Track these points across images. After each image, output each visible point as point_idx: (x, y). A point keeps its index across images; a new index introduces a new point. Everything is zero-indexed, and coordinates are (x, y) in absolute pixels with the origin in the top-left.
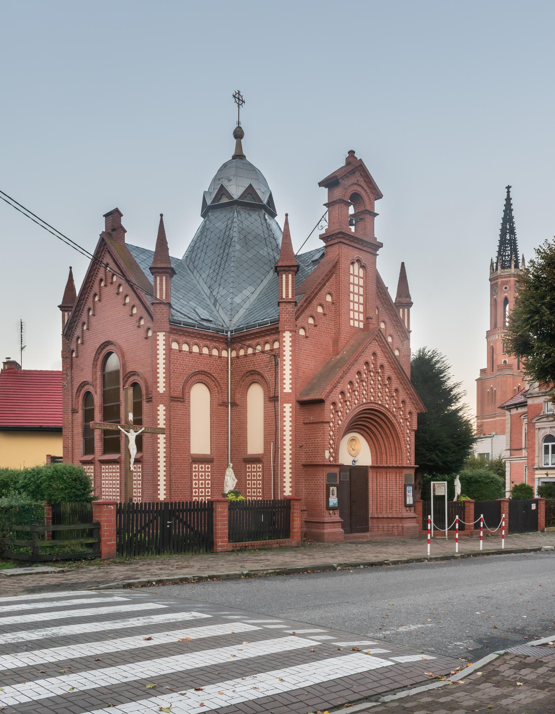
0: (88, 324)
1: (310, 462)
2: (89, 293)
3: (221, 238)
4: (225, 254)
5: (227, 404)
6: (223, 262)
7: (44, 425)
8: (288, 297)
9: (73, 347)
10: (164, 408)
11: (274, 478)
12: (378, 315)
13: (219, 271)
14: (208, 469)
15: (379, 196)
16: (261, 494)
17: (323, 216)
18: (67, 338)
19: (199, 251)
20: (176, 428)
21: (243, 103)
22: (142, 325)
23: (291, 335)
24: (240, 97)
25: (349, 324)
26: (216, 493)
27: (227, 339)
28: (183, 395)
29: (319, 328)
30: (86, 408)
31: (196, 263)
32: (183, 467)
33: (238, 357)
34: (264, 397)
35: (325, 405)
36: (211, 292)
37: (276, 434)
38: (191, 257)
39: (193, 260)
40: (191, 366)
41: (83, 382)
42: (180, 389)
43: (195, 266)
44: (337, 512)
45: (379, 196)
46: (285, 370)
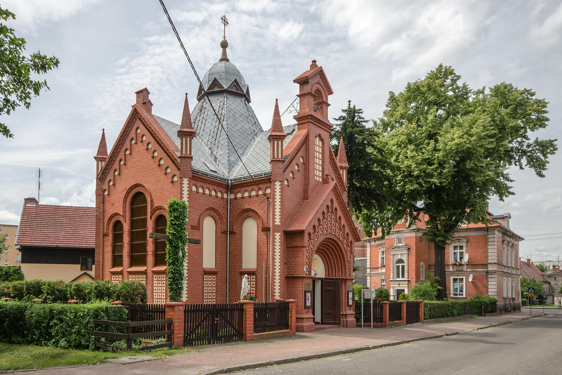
1: (292, 275)
5: (226, 232)
7: (60, 245)
8: (278, 157)
9: (105, 187)
13: (216, 138)
15: (331, 93)
18: (100, 180)
19: (200, 123)
22: (168, 173)
26: (219, 296)
27: (228, 185)
28: (199, 225)
30: (115, 233)
32: (198, 277)
36: (212, 152)
40: (204, 204)
41: (114, 213)
42: (197, 220)
45: (331, 93)
46: (276, 208)
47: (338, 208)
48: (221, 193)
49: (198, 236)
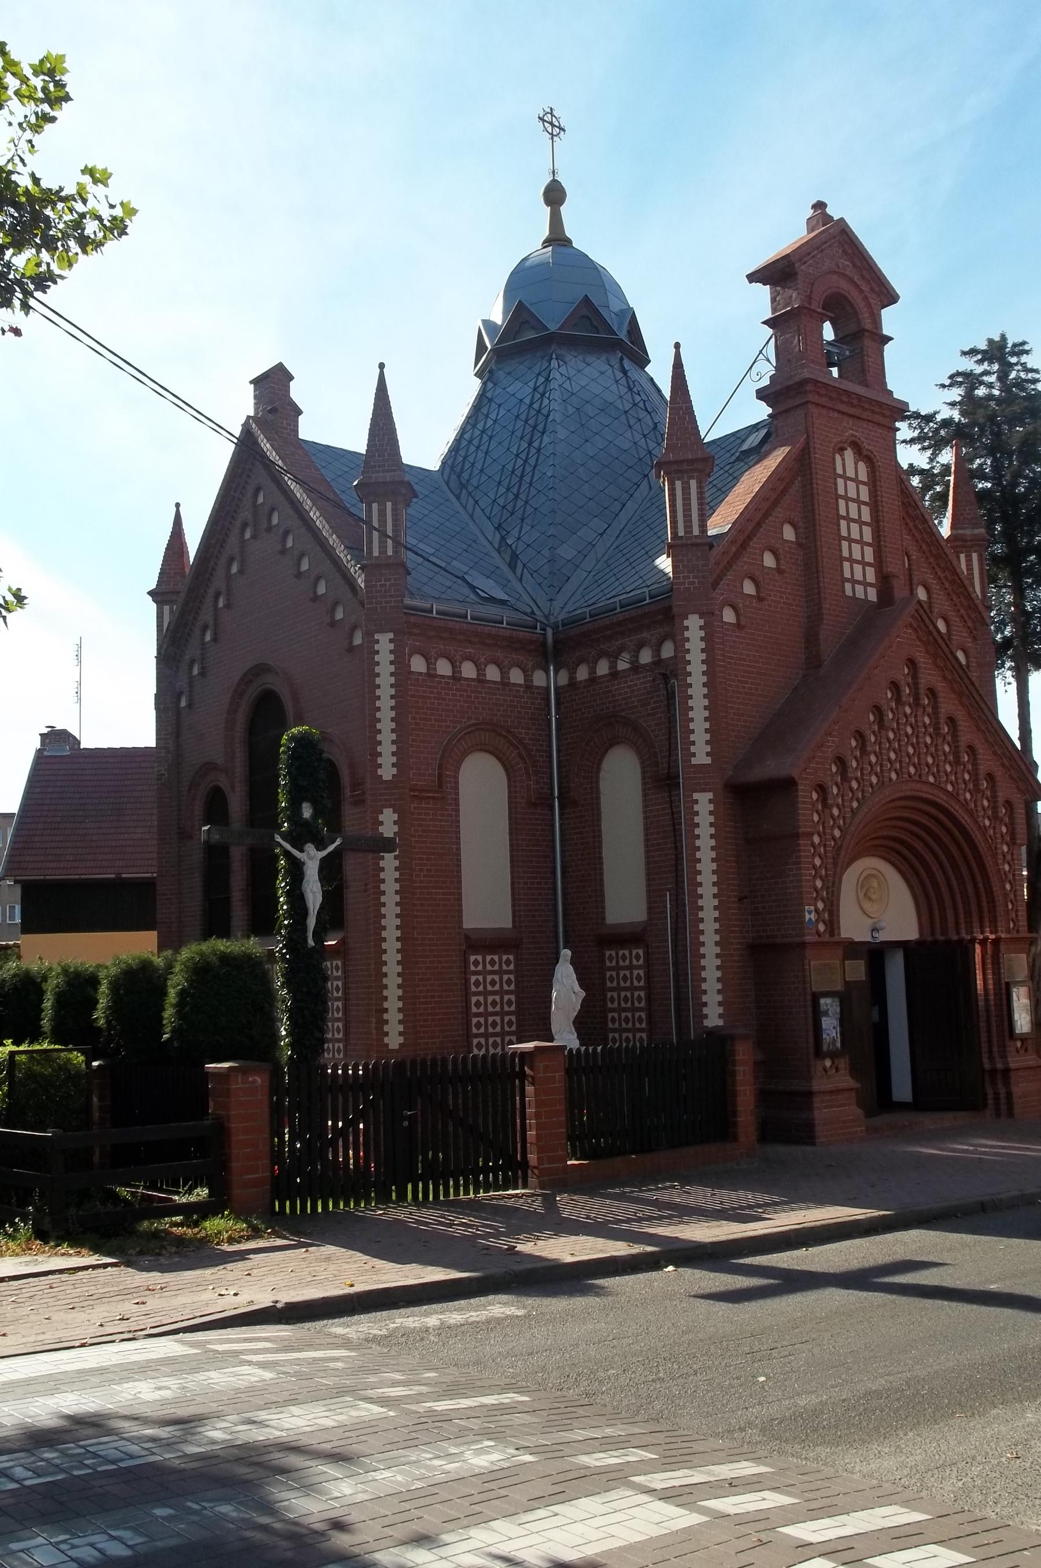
0: (215, 629)
2: (217, 557)
3: (523, 417)
4: (533, 451)
6: (528, 469)
10: (395, 817)
11: (676, 981)
12: (910, 569)
13: (519, 490)
14: (508, 966)
15: (890, 297)
16: (644, 1025)
17: (761, 352)
19: (472, 449)
20: (426, 865)
21: (562, 132)
23: (702, 622)
24: (550, 130)
25: (844, 592)
27: (544, 644)
28: (440, 786)
29: (770, 606)
31: (465, 475)
33: (573, 684)
34: (643, 778)
35: (797, 790)
36: (503, 538)
37: (676, 871)
38: (453, 464)
39: (458, 469)
43: (464, 482)
44: (843, 1063)
47: (940, 686)
48: (501, 670)
49: (441, 821)
